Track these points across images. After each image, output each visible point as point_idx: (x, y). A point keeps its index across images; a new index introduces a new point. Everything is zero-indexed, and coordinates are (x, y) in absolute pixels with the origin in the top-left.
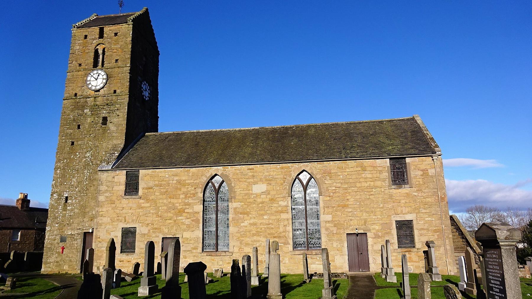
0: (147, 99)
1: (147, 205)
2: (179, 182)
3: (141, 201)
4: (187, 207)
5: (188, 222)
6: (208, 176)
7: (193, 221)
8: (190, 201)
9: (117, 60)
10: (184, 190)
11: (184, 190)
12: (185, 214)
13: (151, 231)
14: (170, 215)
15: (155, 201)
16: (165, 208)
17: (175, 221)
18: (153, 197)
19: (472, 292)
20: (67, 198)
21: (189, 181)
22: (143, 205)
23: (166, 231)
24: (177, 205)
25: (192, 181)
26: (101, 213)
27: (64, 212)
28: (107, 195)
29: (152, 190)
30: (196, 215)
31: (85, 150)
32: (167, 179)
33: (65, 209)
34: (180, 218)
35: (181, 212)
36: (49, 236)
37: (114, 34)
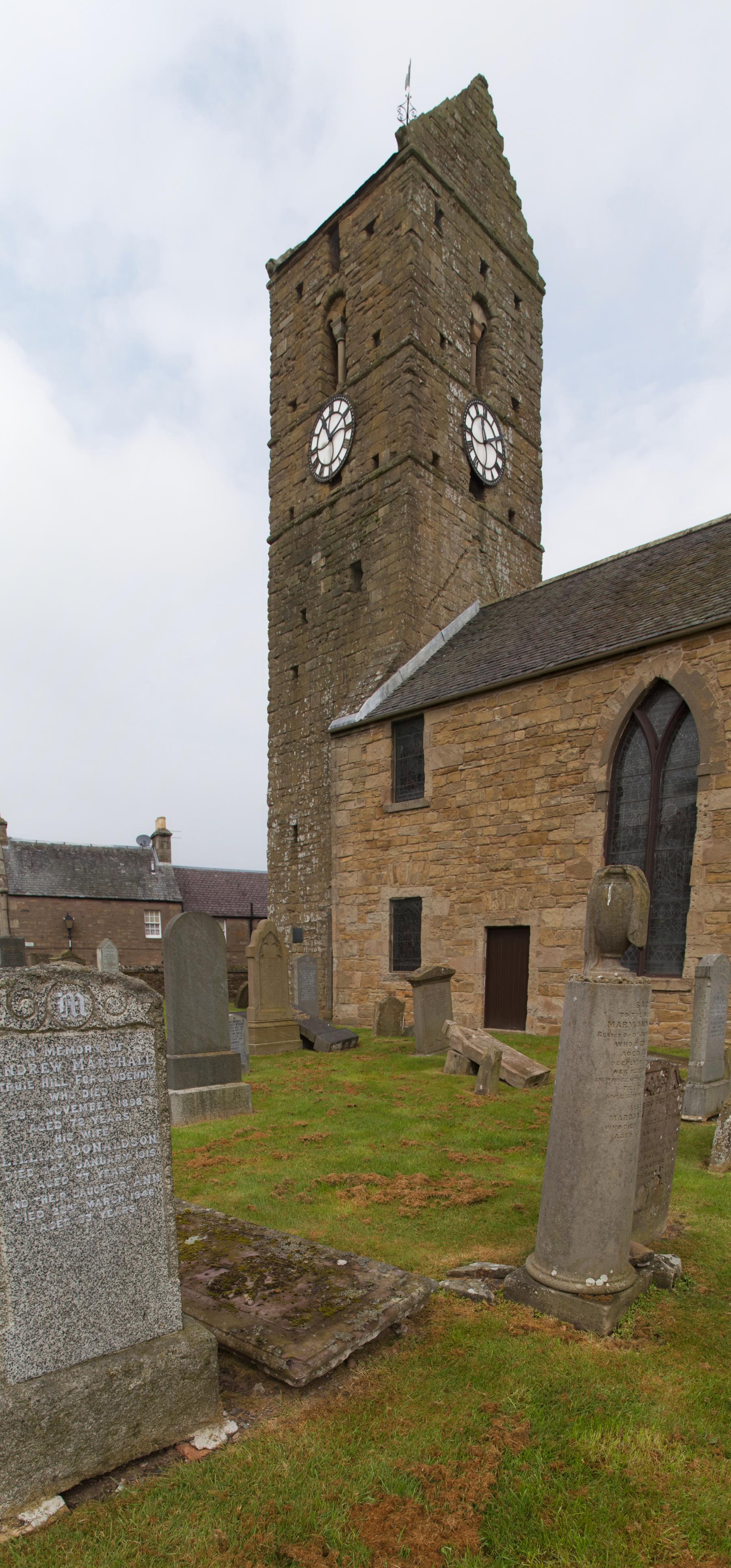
0: (341, 406)
1: (446, 826)
2: (532, 732)
3: (431, 816)
4: (556, 822)
5: (552, 873)
6: (626, 693)
7: (570, 870)
8: (568, 799)
9: (376, 337)
10: (548, 759)
11: (548, 759)
12: (546, 850)
13: (457, 907)
14: (505, 853)
15: (463, 813)
16: (493, 830)
17: (519, 874)
18: (460, 799)
19: (460, 462)
20: (295, 827)
21: (562, 727)
22: (435, 828)
23: (493, 906)
24: (527, 818)
25: (573, 724)
26: (344, 860)
27: (294, 867)
28: (351, 805)
29: (455, 777)
30: (581, 850)
31: (320, 686)
32: (498, 731)
33: (294, 860)
34: (533, 863)
35: (540, 839)
36: (540, 942)
37: (364, 235)
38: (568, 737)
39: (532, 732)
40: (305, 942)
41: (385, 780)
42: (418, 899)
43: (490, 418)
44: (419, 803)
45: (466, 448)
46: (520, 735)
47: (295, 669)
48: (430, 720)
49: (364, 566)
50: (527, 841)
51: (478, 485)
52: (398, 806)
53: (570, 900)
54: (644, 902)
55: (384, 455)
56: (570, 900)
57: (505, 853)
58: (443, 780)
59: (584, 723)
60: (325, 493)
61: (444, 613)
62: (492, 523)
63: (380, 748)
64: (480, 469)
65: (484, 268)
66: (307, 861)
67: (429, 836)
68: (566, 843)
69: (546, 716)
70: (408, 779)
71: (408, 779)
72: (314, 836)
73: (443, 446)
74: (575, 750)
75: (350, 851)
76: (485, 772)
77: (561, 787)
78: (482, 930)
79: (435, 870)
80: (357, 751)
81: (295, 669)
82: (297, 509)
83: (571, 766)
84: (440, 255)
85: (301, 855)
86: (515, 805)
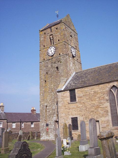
1: (81, 105)
2: (95, 92)
3: (78, 104)
4: (101, 104)
5: (102, 112)
10: (98, 96)
11: (98, 96)
16: (90, 106)
18: (83, 101)
20: (46, 106)
25: (101, 91)
33: (46, 111)
35: (98, 107)
38: (101, 93)
39: (95, 92)
40: (49, 126)
41: (69, 99)
42: (77, 118)
43: (74, 49)
44: (76, 102)
45: (72, 52)
46: (93, 92)
47: (45, 81)
48: (76, 90)
49: (59, 67)
50: (96, 107)
51: (73, 57)
52: (72, 103)
53: (105, 116)
54: (75, 107)
55: (61, 54)
56: (105, 116)
57: (92, 109)
58: (80, 99)
59: (103, 91)
60: (51, 58)
61: (71, 73)
62: (75, 61)
63: (68, 93)
64: (73, 55)
65: (71, 32)
66: (49, 112)
67: (78, 107)
68: (103, 107)
69: (97, 90)
70: (73, 98)
71: (73, 98)
72: (51, 107)
73: (69, 52)
74: (102, 94)
75: (62, 110)
76: (87, 97)
77: (101, 99)
78: (71, 119)
79: (79, 112)
80: (63, 94)
81: (45, 81)
82: (45, 59)
83: (102, 96)
84: (67, 32)
85: (48, 111)
86: (94, 102)
